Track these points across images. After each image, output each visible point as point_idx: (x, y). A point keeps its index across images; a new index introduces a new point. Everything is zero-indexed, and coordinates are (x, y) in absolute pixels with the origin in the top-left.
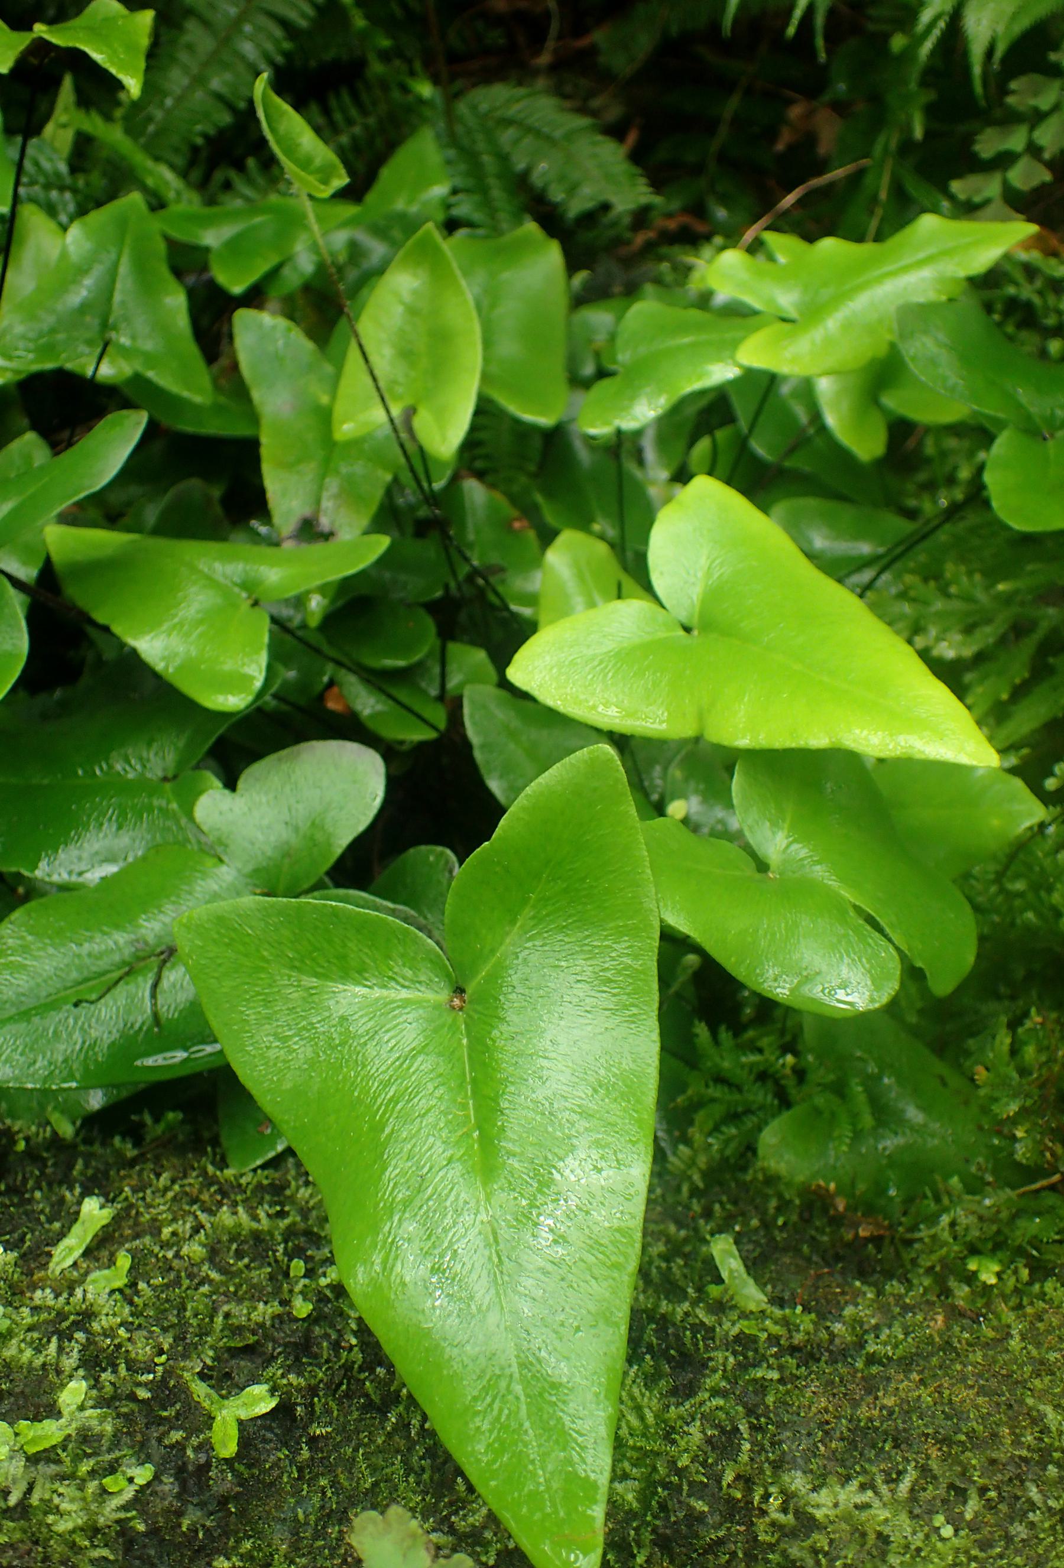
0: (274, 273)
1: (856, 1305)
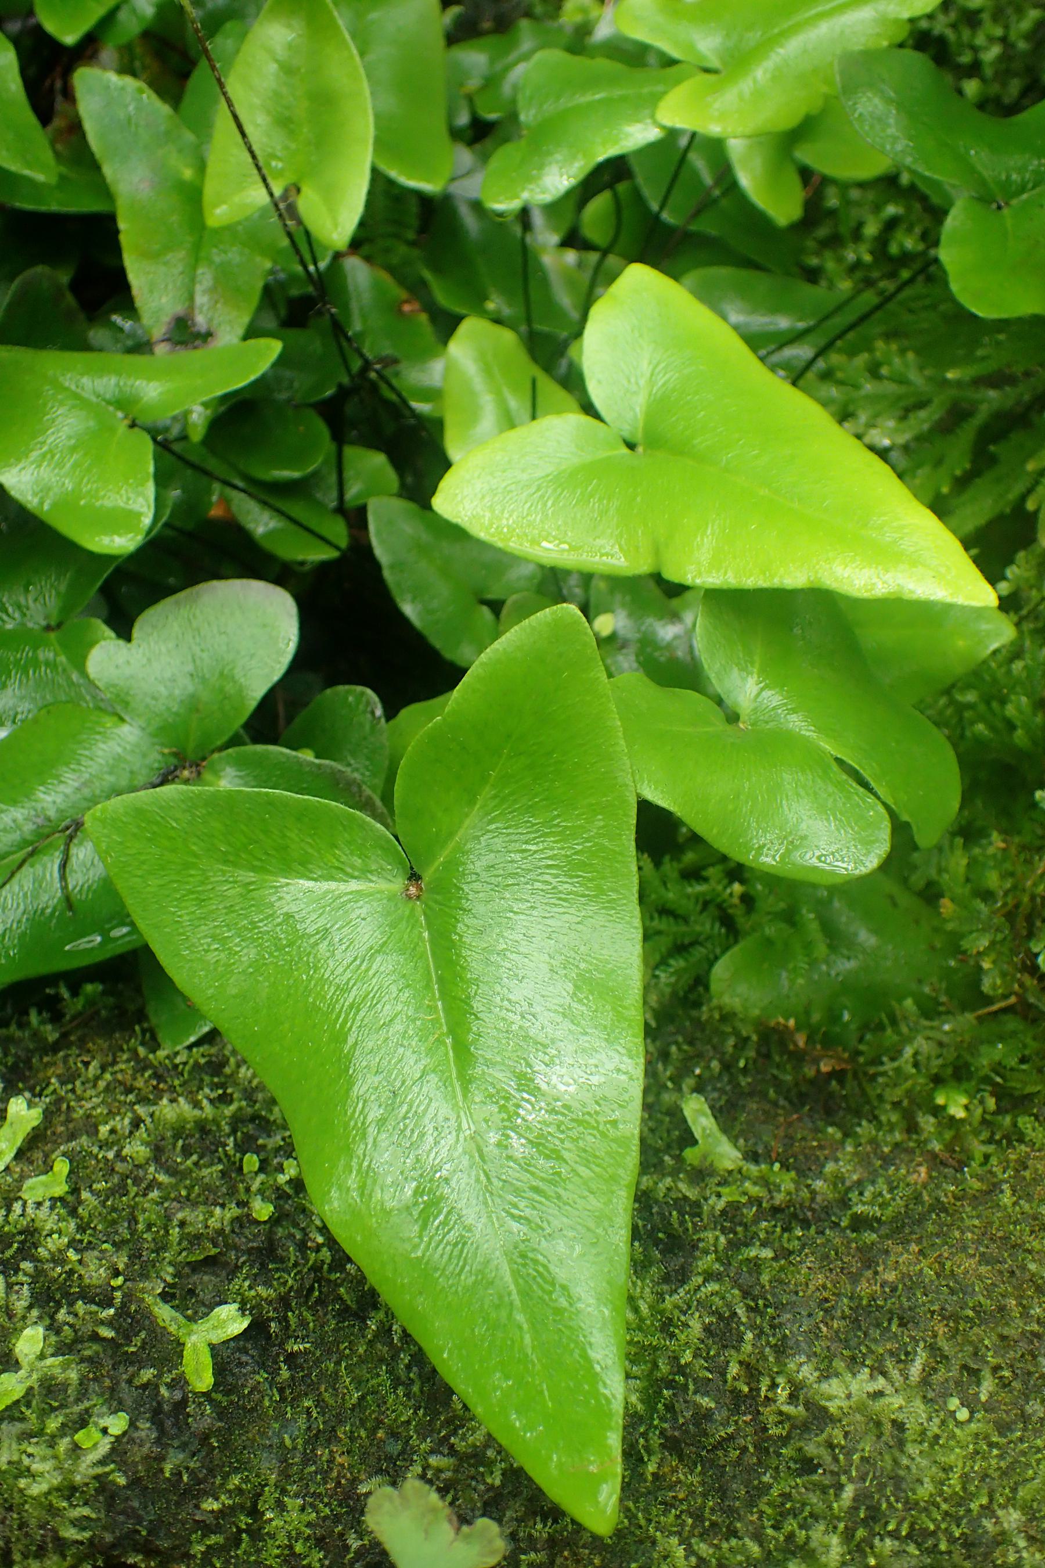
0: (109, 19)
1: (837, 1160)
